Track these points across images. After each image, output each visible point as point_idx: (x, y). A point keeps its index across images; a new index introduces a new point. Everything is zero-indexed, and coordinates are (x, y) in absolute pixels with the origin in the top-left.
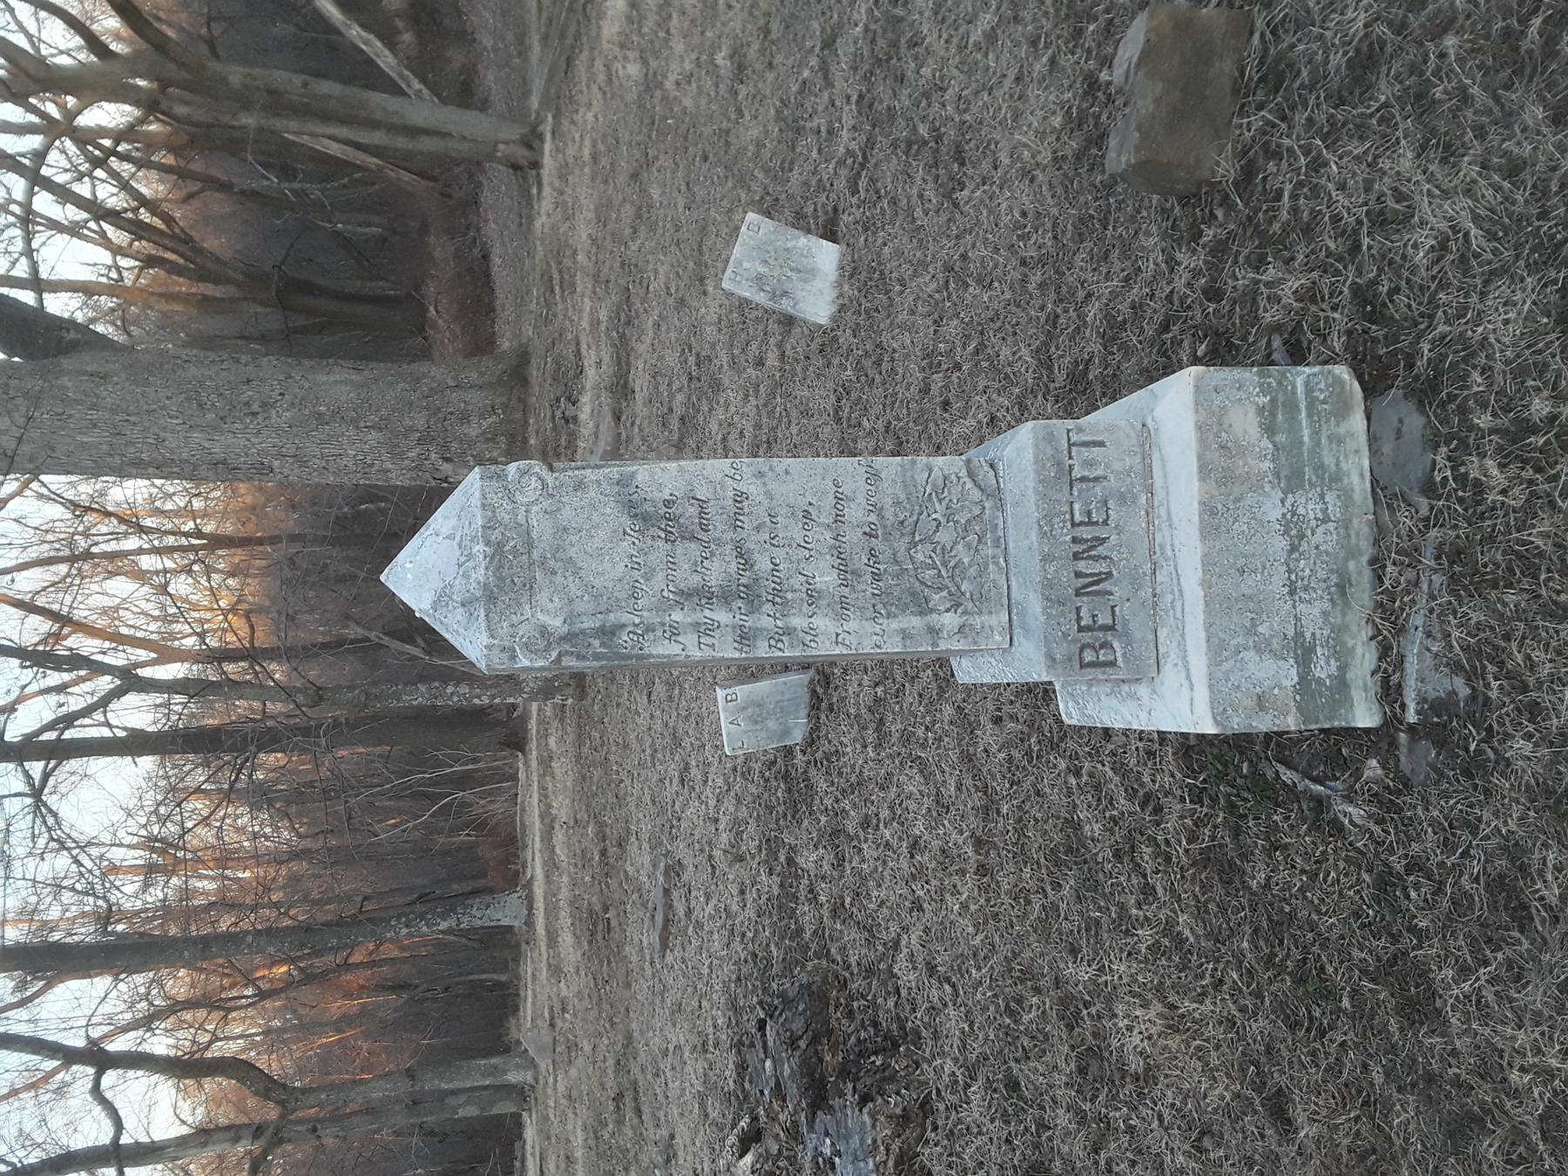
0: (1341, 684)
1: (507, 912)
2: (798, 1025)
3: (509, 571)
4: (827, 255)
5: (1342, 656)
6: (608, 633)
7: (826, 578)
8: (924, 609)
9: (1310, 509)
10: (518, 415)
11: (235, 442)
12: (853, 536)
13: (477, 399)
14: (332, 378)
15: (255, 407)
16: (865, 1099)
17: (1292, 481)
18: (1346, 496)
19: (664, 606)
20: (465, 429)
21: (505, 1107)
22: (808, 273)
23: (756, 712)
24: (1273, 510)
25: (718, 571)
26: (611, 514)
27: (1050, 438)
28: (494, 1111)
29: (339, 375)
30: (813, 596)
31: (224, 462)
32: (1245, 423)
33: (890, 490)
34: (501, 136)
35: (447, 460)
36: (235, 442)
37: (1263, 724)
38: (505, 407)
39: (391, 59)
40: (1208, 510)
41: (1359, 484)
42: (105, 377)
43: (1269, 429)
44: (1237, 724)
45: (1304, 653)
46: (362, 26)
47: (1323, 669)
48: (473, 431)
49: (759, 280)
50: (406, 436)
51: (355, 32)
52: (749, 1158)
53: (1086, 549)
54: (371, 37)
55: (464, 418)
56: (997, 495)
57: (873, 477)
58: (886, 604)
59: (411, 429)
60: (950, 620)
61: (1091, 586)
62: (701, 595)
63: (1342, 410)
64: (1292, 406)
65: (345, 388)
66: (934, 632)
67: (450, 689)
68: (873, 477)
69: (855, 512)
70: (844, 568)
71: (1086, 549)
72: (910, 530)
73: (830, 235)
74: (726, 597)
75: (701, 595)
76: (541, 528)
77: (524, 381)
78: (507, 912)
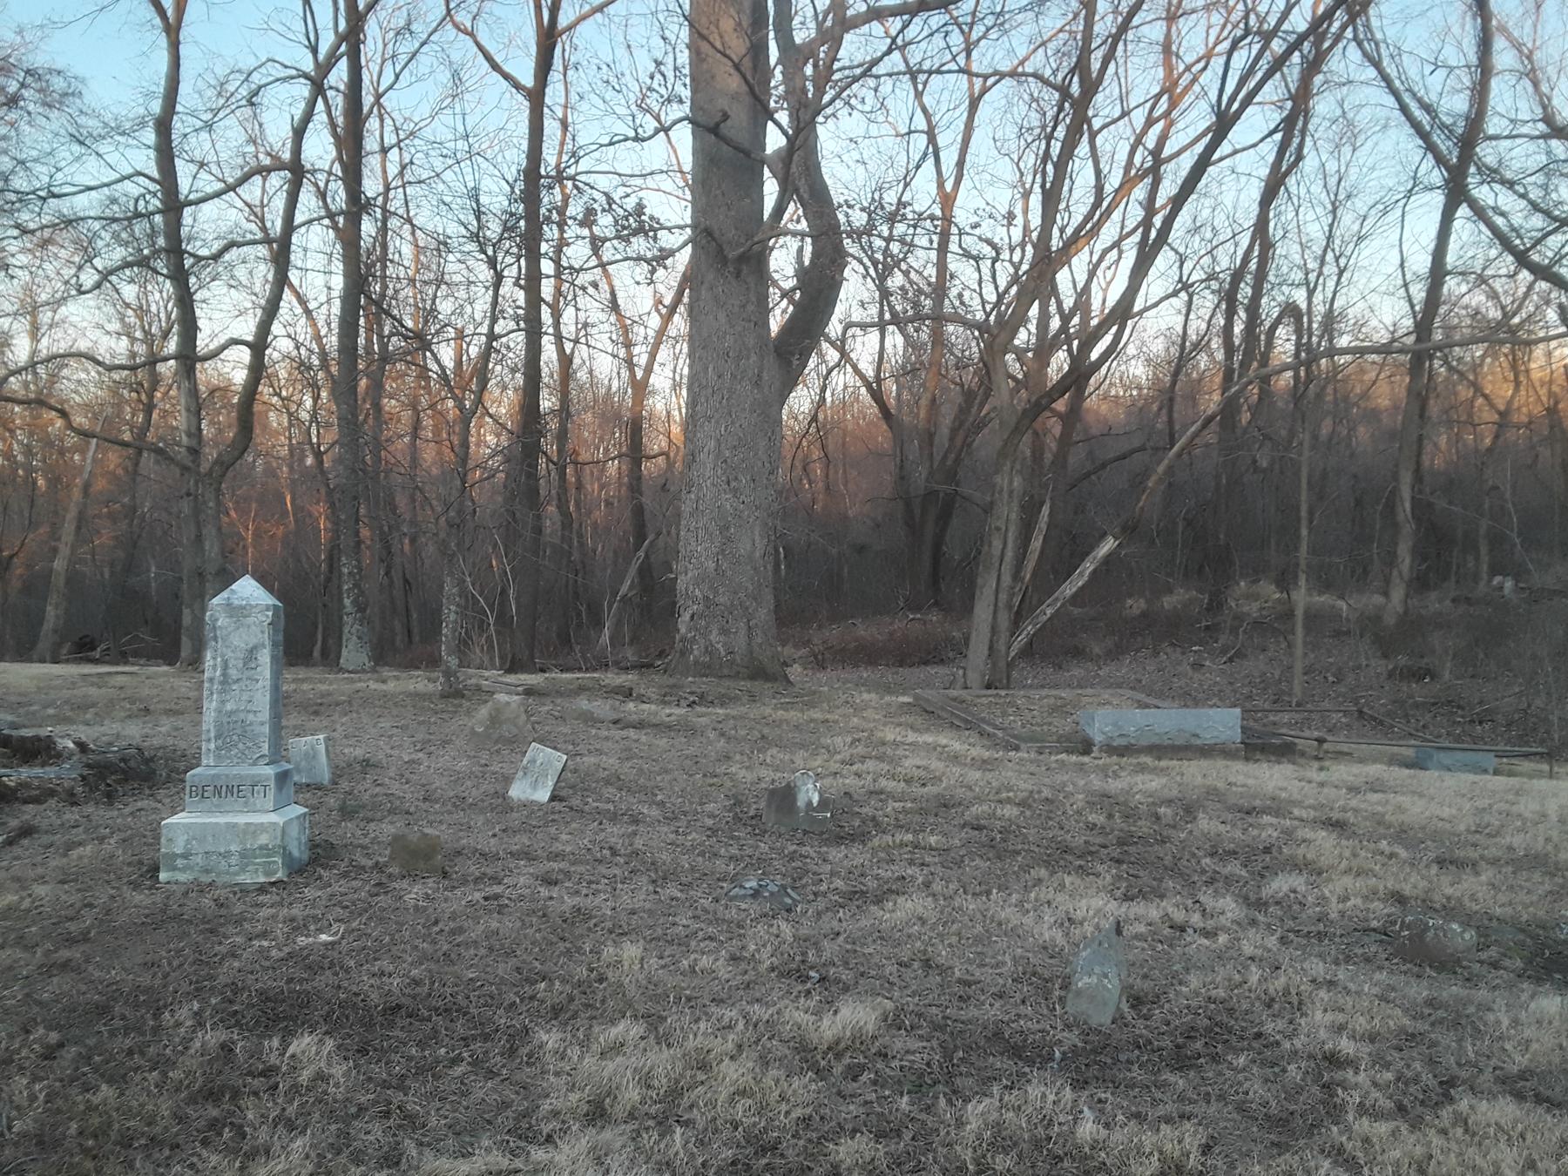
0: (175, 869)
1: (353, 653)
2: (132, 764)
3: (238, 612)
4: (543, 795)
5: (183, 870)
6: (215, 639)
7: (229, 707)
8: (217, 737)
9: (233, 861)
10: (726, 672)
11: (707, 465)
12: (242, 716)
13: (740, 642)
14: (757, 538)
15: (733, 484)
16: (84, 778)
17: (243, 854)
18: (237, 874)
19: (223, 656)
20: (715, 632)
21: (185, 651)
22: (535, 786)
23: (311, 756)
24: (233, 848)
25: (233, 673)
26: (253, 641)
27: (268, 779)
28: (184, 639)
29: (760, 544)
30: (223, 702)
31: (694, 460)
32: (263, 839)
33: (258, 729)
34: (969, 673)
35: (692, 617)
36: (707, 465)
37: (163, 840)
38: (733, 662)
39: (1068, 593)
40: (235, 825)
41: (241, 879)
42: (757, 384)
43: (261, 848)
44: (164, 831)
45: (185, 856)
46: (1095, 571)
47: (180, 862)
48: (714, 637)
49: (533, 761)
50: (711, 588)
51: (1088, 567)
52: (71, 745)
53: (230, 789)
54: (1086, 578)
55: (724, 631)
56: (254, 764)
57: (262, 724)
58: (219, 726)
59: (716, 593)
60: (212, 746)
61: (217, 791)
62: (225, 666)
63: (267, 874)
64: (269, 856)
65: (748, 547)
66: (209, 740)
67: (453, 608)
68: (262, 724)
69: (251, 717)
70: (231, 713)
71: (230, 789)
72: (243, 735)
73: (553, 798)
74: (224, 675)
75: (225, 666)
76: (251, 620)
77: (752, 677)
78: (353, 653)
